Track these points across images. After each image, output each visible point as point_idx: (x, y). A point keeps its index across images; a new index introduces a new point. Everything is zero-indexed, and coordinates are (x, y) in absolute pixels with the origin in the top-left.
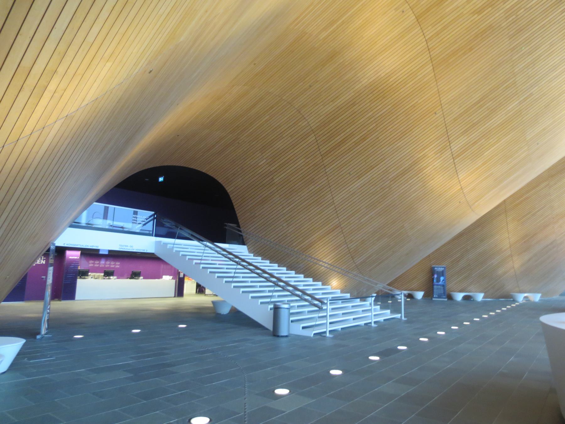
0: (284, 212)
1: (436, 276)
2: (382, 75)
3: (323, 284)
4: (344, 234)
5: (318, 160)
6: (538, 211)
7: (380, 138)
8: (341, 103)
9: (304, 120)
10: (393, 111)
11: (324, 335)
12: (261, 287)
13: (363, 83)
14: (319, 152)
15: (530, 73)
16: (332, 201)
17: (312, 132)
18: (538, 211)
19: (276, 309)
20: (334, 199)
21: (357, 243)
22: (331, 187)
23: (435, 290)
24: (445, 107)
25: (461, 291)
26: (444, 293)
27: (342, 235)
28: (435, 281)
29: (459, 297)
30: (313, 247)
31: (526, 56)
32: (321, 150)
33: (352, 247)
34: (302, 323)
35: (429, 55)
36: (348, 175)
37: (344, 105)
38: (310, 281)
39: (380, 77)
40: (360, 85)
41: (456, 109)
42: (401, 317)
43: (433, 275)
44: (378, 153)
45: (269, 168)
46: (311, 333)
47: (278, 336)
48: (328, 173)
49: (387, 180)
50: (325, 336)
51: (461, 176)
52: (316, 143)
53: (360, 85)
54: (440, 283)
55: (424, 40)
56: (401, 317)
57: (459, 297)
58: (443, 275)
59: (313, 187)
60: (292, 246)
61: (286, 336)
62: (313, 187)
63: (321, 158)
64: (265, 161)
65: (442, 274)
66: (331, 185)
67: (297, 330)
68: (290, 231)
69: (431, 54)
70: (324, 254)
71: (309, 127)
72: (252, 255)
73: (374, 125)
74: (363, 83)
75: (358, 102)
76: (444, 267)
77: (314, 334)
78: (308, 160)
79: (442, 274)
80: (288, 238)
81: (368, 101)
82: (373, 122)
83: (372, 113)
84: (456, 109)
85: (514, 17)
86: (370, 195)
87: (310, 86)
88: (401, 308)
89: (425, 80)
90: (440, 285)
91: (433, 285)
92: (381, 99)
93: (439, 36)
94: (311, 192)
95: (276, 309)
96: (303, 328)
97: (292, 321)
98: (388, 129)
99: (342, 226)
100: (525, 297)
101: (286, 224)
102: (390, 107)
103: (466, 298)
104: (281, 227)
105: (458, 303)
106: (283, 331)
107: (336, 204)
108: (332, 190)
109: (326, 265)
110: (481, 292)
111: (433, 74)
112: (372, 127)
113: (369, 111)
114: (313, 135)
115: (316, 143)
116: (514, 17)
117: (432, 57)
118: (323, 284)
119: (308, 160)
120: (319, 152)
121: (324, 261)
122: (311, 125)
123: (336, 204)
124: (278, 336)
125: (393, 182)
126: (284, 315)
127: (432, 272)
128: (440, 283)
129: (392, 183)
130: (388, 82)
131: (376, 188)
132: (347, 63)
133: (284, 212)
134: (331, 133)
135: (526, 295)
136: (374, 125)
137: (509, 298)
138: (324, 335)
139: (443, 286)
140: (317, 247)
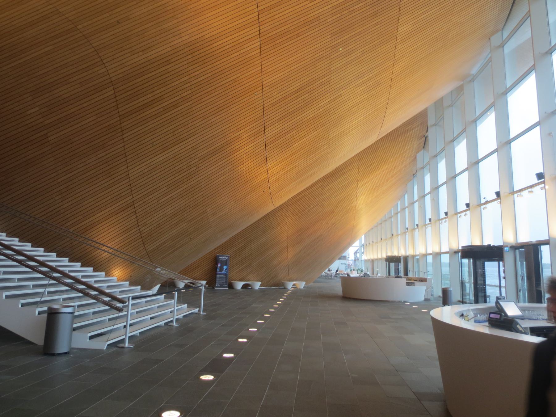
0: (59, 180)
1: (219, 265)
2: (207, 36)
3: (106, 275)
4: (137, 215)
5: (116, 120)
6: (313, 207)
7: (193, 109)
8: (153, 56)
9: (103, 66)
10: (212, 81)
11: (121, 345)
12: (20, 280)
13: (184, 39)
14: (116, 111)
15: (343, 75)
16: (127, 173)
17: (111, 84)
18: (313, 207)
19: (52, 316)
20: (130, 172)
21: (152, 227)
22: (128, 158)
23: (217, 279)
24: (265, 89)
25: (241, 280)
26: (226, 282)
27: (135, 216)
28: (218, 270)
29: (239, 285)
30: (96, 228)
31: (342, 57)
32: (120, 110)
33: (144, 231)
34: (90, 330)
35: (258, 29)
36: (151, 145)
37: (155, 60)
38: (89, 271)
39: (204, 38)
40: (180, 40)
41: (276, 93)
42: (199, 311)
43: (217, 264)
44: (190, 125)
45: (41, 120)
46: (102, 345)
47: (53, 355)
48: (125, 140)
49: (195, 157)
50: (123, 348)
51: (270, 164)
52: (114, 100)
53: (180, 40)
54: (223, 272)
55: (256, 10)
56: (199, 311)
57: (239, 285)
58: (226, 265)
59: (104, 154)
60: (66, 225)
61: (66, 353)
62: (104, 154)
63: (118, 119)
64: (37, 109)
65: (225, 263)
66: (127, 154)
67: (82, 341)
68: (65, 206)
69: (261, 28)
70: (108, 236)
71: (108, 77)
72: (5, 234)
73: (189, 92)
74: (184, 39)
75: (173, 60)
76: (228, 257)
77: (108, 345)
78: (101, 119)
79: (225, 263)
80: (62, 215)
81: (186, 62)
82: (189, 88)
83: (187, 77)
84: (276, 93)
85: (339, 15)
86: (174, 173)
87: (118, 22)
88: (200, 303)
89: (250, 55)
90: (223, 274)
91: (216, 274)
92: (200, 63)
93: (272, 11)
94: (100, 160)
95: (52, 316)
96: (91, 337)
97: (74, 329)
98: (204, 100)
99: (136, 205)
100: (294, 285)
101: (60, 197)
102: (209, 75)
103: (245, 287)
104: (52, 200)
105: (237, 293)
106: (62, 347)
107: (131, 179)
108: (128, 161)
109: (111, 251)
110: (258, 281)
111: (259, 51)
112: (186, 94)
113: (185, 75)
114: (112, 88)
115: (114, 100)
116: (339, 15)
117: (261, 31)
118: (106, 275)
119: (101, 119)
120: (116, 111)
121: (109, 245)
122: (111, 75)
123: (131, 179)
124: (53, 355)
125: (201, 161)
126: (64, 324)
127: (216, 260)
128: (223, 272)
129: (200, 162)
130: (211, 47)
131: (182, 165)
132: (169, 8)
133: (59, 180)
134: (136, 90)
135: (294, 283)
136: (189, 92)
137: (280, 286)
138: (121, 345)
139: (226, 275)
140: (101, 228)
